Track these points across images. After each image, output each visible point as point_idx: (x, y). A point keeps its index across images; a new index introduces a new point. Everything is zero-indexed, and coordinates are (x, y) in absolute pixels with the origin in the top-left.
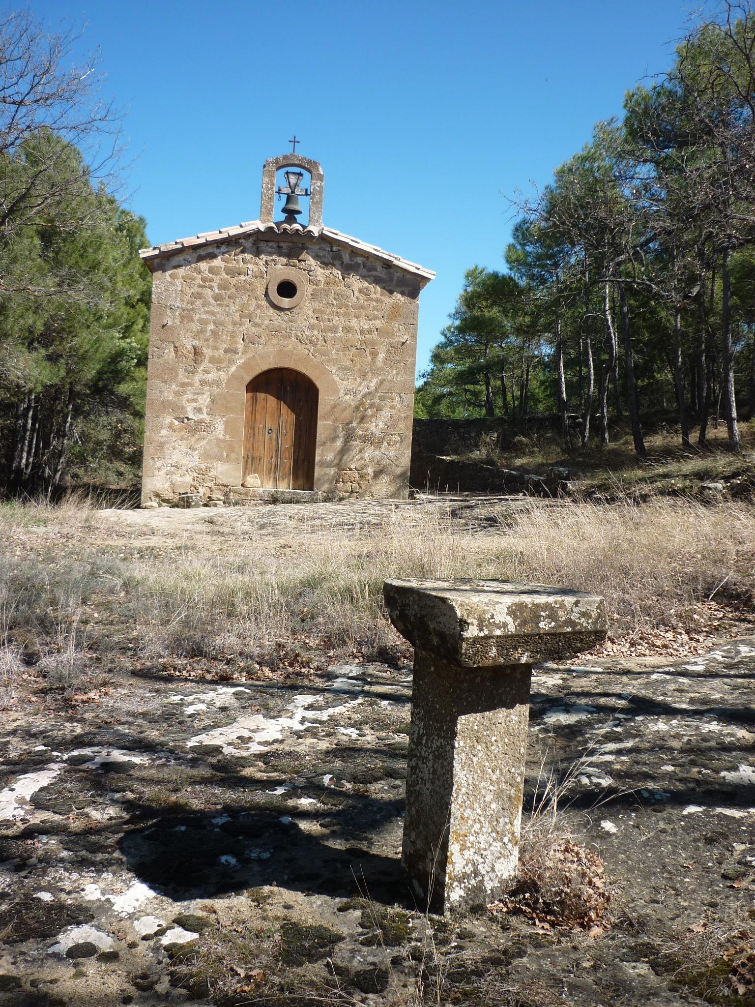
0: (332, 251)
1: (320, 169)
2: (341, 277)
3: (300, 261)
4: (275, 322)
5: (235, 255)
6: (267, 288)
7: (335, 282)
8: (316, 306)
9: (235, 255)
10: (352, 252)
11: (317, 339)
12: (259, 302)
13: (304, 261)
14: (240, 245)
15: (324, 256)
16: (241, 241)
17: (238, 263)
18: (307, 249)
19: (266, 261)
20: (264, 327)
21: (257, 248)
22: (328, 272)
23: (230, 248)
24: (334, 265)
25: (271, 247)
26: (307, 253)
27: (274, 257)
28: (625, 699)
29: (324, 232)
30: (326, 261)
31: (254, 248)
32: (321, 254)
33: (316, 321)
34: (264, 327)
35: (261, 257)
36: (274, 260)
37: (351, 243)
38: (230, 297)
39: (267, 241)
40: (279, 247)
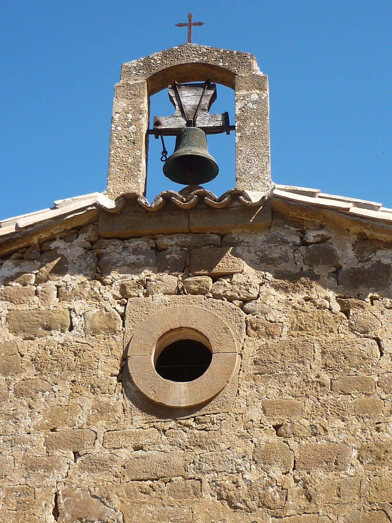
0: (304, 243)
1: (255, 66)
2: (337, 307)
3: (216, 278)
4: (153, 453)
5: (38, 281)
6: (125, 359)
7: (321, 320)
8: (273, 393)
9: (38, 281)
10: (362, 238)
11: (283, 490)
12: (104, 399)
13: (229, 275)
14: (53, 254)
15: (284, 258)
16: (53, 245)
17: (44, 296)
18: (235, 244)
19: (123, 287)
20: (117, 468)
21: (99, 257)
22: (298, 297)
23: (26, 265)
24: (315, 278)
25: (136, 251)
26: (234, 254)
27: (146, 273)
28: (76, 229)
29: (276, 192)
30: (293, 269)
31: (90, 260)
32: (276, 253)
33: (274, 439)
34: (117, 468)
35: (108, 279)
36: (144, 284)
37: (355, 210)
38: (19, 393)
39: (122, 239)
40: (157, 249)
